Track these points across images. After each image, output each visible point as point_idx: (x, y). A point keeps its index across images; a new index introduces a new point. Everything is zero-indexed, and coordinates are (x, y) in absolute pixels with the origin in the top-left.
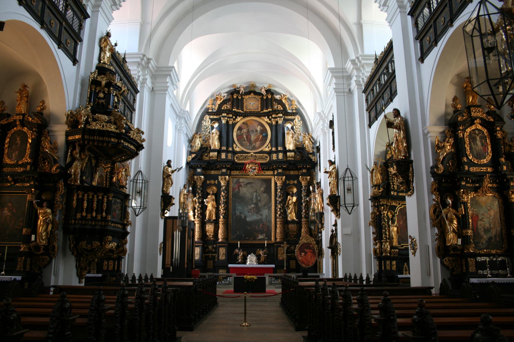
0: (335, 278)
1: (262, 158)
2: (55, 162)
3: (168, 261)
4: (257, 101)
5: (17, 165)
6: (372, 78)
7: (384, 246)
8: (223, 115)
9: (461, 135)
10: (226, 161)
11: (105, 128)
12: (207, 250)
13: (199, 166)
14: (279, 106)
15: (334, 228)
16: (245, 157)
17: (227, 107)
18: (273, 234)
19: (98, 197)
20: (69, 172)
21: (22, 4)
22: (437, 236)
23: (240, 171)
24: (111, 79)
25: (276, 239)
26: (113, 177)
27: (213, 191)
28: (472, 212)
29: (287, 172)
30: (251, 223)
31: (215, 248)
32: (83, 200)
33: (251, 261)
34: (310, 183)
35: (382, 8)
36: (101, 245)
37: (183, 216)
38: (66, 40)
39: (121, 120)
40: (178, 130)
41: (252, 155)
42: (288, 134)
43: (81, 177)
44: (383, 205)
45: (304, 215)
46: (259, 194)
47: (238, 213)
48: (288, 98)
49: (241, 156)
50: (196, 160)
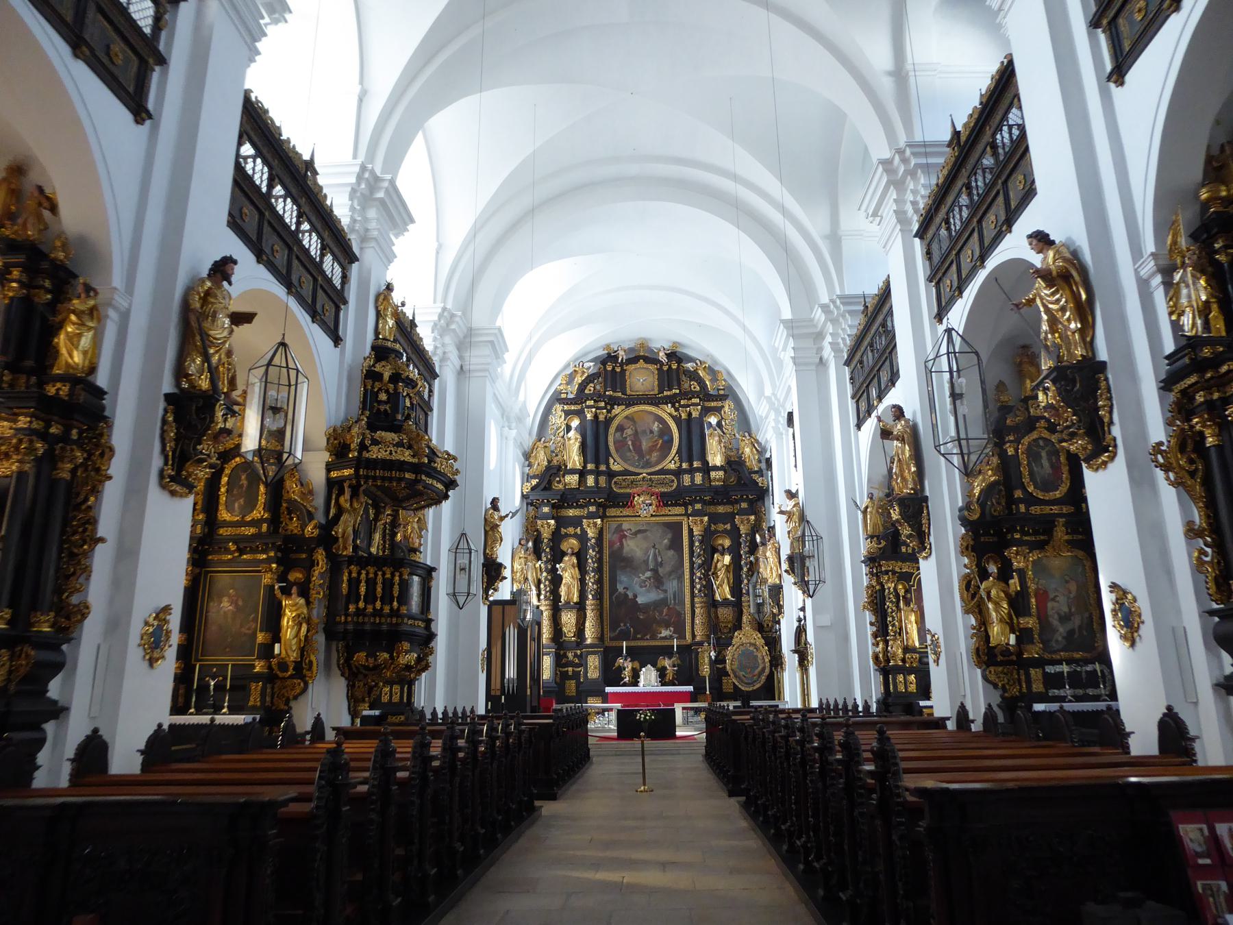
2: (311, 517)
3: (496, 684)
9: (1011, 452)
10: (597, 489)
11: (395, 457)
15: (801, 614)
16: (632, 482)
17: (594, 387)
18: (688, 628)
19: (384, 574)
20: (333, 533)
21: (81, 56)
22: (974, 629)
25: (694, 636)
26: (397, 533)
27: (572, 548)
29: (712, 509)
31: (580, 657)
33: (648, 680)
34: (756, 528)
35: (871, 219)
38: (323, 307)
39: (421, 440)
41: (644, 477)
43: (354, 541)
44: (887, 572)
46: (659, 552)
47: (620, 588)
49: (624, 480)
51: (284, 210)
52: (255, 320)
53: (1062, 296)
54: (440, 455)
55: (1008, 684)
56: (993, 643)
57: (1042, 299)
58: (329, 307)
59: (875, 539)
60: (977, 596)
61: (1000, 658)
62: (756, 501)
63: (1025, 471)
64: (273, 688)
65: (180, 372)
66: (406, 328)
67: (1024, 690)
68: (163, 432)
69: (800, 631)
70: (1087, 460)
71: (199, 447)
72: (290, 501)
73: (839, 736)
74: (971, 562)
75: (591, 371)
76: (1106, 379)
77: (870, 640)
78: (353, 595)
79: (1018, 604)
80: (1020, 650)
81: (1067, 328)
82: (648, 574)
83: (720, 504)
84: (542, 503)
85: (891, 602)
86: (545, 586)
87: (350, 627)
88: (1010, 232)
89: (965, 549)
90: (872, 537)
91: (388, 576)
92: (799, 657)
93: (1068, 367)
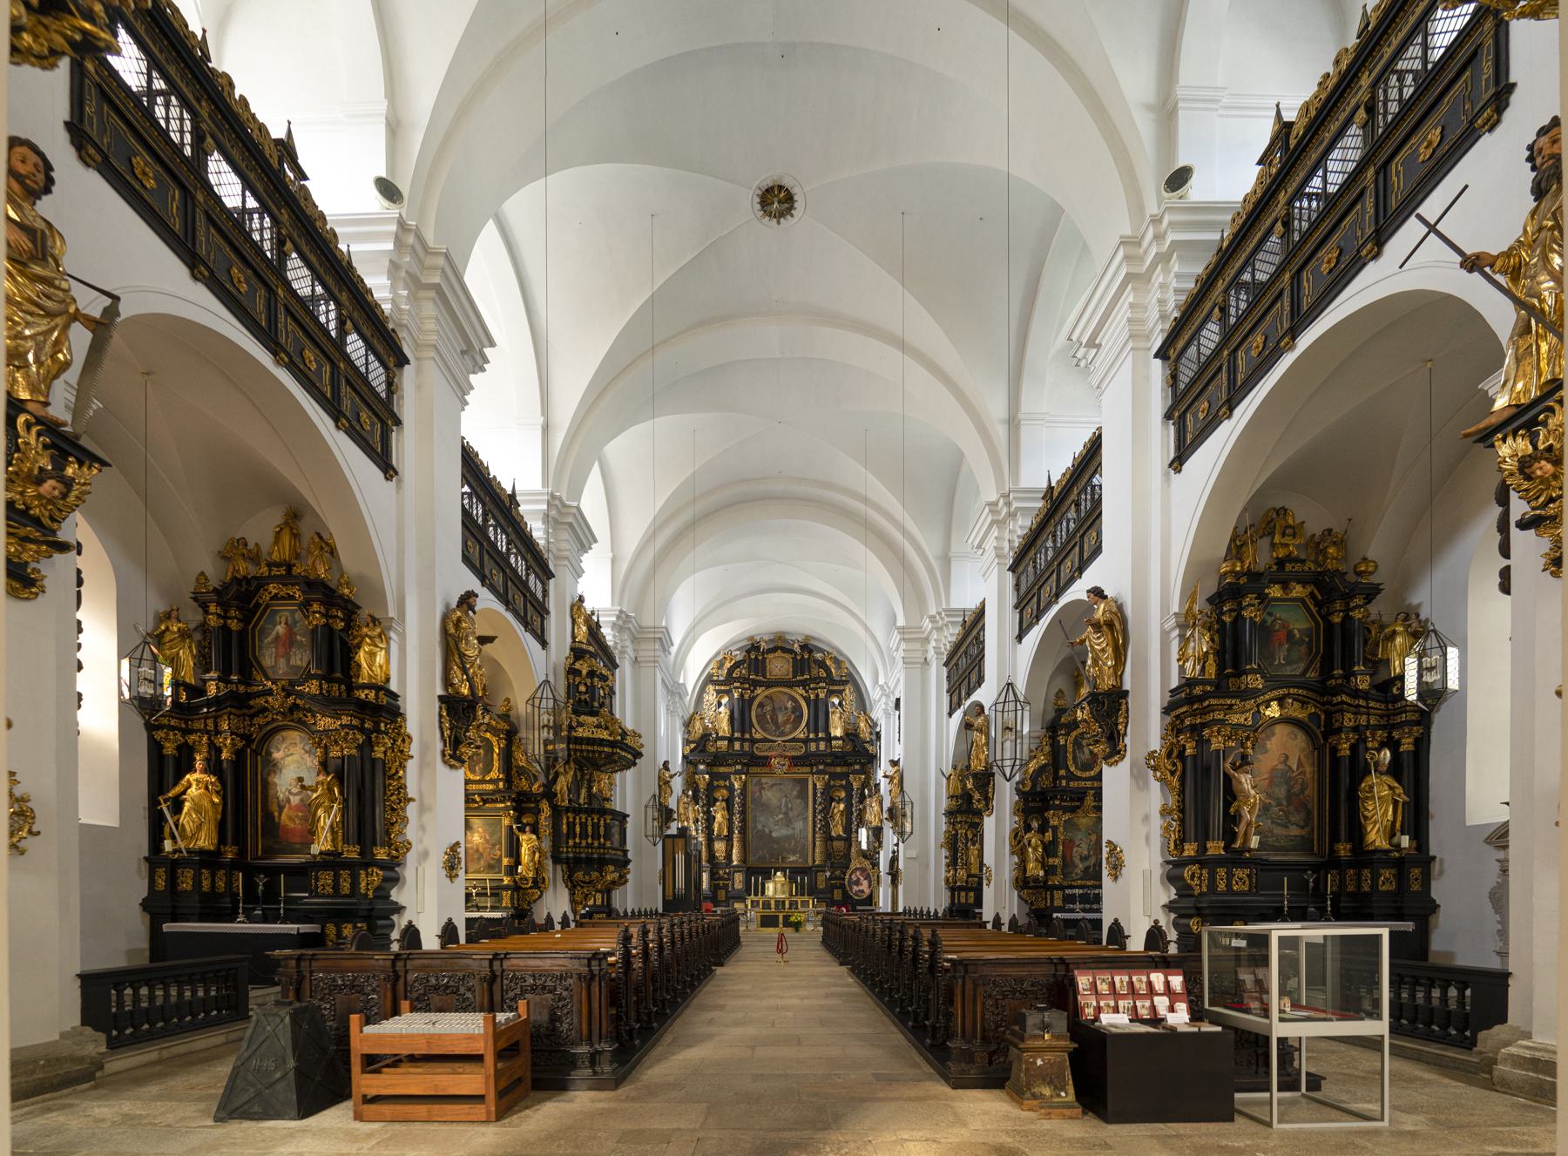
0: (895, 913)
5: (482, 781)
6: (957, 647)
8: (735, 684)
9: (1062, 742)
10: (742, 754)
12: (717, 876)
15: (896, 848)
19: (592, 819)
29: (832, 769)
30: (777, 841)
32: (575, 824)
34: (865, 784)
36: (602, 876)
37: (683, 832)
42: (833, 713)
47: (760, 827)
51: (367, 369)
56: (1028, 874)
57: (1090, 641)
61: (1032, 884)
63: (1070, 756)
65: (447, 681)
66: (594, 630)
67: (1048, 904)
68: (441, 722)
69: (894, 860)
70: (1105, 758)
73: (911, 932)
75: (739, 658)
76: (1127, 703)
77: (944, 868)
78: (571, 833)
79: (1049, 849)
81: (1105, 664)
82: (781, 816)
83: (838, 765)
84: (699, 762)
87: (571, 855)
89: (1016, 812)
90: (952, 797)
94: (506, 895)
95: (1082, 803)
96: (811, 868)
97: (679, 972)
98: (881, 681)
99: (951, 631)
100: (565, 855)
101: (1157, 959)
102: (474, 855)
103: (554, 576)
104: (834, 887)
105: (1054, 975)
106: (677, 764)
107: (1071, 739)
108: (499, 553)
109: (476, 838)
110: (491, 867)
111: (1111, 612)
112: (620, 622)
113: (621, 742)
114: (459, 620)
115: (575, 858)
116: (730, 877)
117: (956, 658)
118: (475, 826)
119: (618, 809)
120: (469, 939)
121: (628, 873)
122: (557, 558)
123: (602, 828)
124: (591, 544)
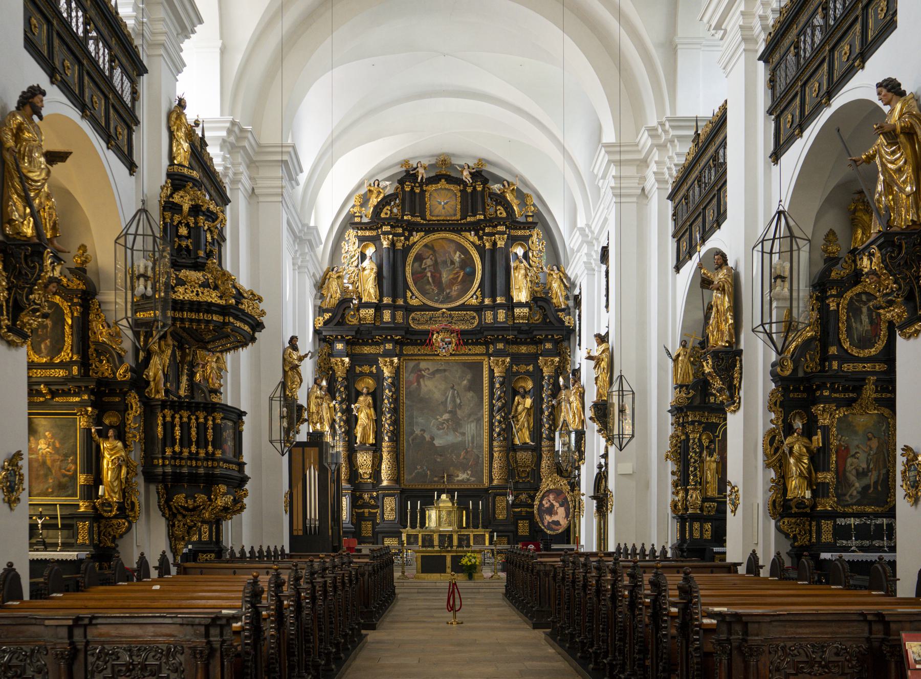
1: (463, 320)
4: (454, 198)
5: (50, 365)
6: (687, 171)
7: (691, 497)
9: (833, 307)
13: (339, 337)
14: (499, 207)
15: (603, 461)
16: (431, 319)
17: (391, 211)
19: (197, 419)
20: (144, 376)
23: (419, 347)
24: (199, 199)
25: (491, 480)
26: (196, 373)
27: (367, 388)
28: (838, 443)
29: (514, 349)
30: (442, 451)
32: (173, 426)
34: (560, 370)
35: (713, 32)
36: (210, 499)
37: (316, 439)
40: (299, 268)
41: (444, 313)
42: (516, 268)
45: (546, 434)
46: (458, 393)
47: (418, 431)
48: (518, 190)
50: (331, 325)
52: (68, 160)
53: (902, 155)
54: (245, 295)
55: (799, 534)
56: (790, 496)
57: (881, 157)
58: (123, 131)
59: (684, 389)
60: (780, 451)
61: (794, 510)
62: (563, 340)
63: (843, 327)
64: (99, 527)
66: (198, 148)
67: (814, 540)
69: (601, 477)
70: (901, 328)
71: (31, 297)
72: (97, 343)
74: (778, 419)
75: (390, 191)
77: (670, 489)
78: (169, 439)
79: (818, 460)
80: (815, 502)
81: (902, 190)
83: (522, 343)
85: (695, 453)
86: (340, 427)
87: (169, 470)
88: (863, 68)
89: (772, 406)
90: (681, 386)
91: (202, 420)
92: (598, 503)
93: (897, 234)
94: (83, 527)
95: (859, 395)
96: (486, 490)
97: (321, 641)
98: (581, 222)
99: (678, 150)
100: (160, 470)
101: (869, 618)
102: (41, 468)
103: (146, 72)
104: (518, 517)
105: (868, 640)
106: (307, 343)
107: (844, 302)
108: (74, 35)
109: (43, 446)
110: (63, 487)
111: (911, 115)
112: (232, 139)
113: (235, 307)
114: (20, 129)
115: (174, 474)
116: (378, 504)
117: (685, 187)
118: (41, 429)
119: (229, 404)
120: (36, 593)
121: (246, 495)
122: (152, 45)
123: (210, 431)
124: (194, 26)
